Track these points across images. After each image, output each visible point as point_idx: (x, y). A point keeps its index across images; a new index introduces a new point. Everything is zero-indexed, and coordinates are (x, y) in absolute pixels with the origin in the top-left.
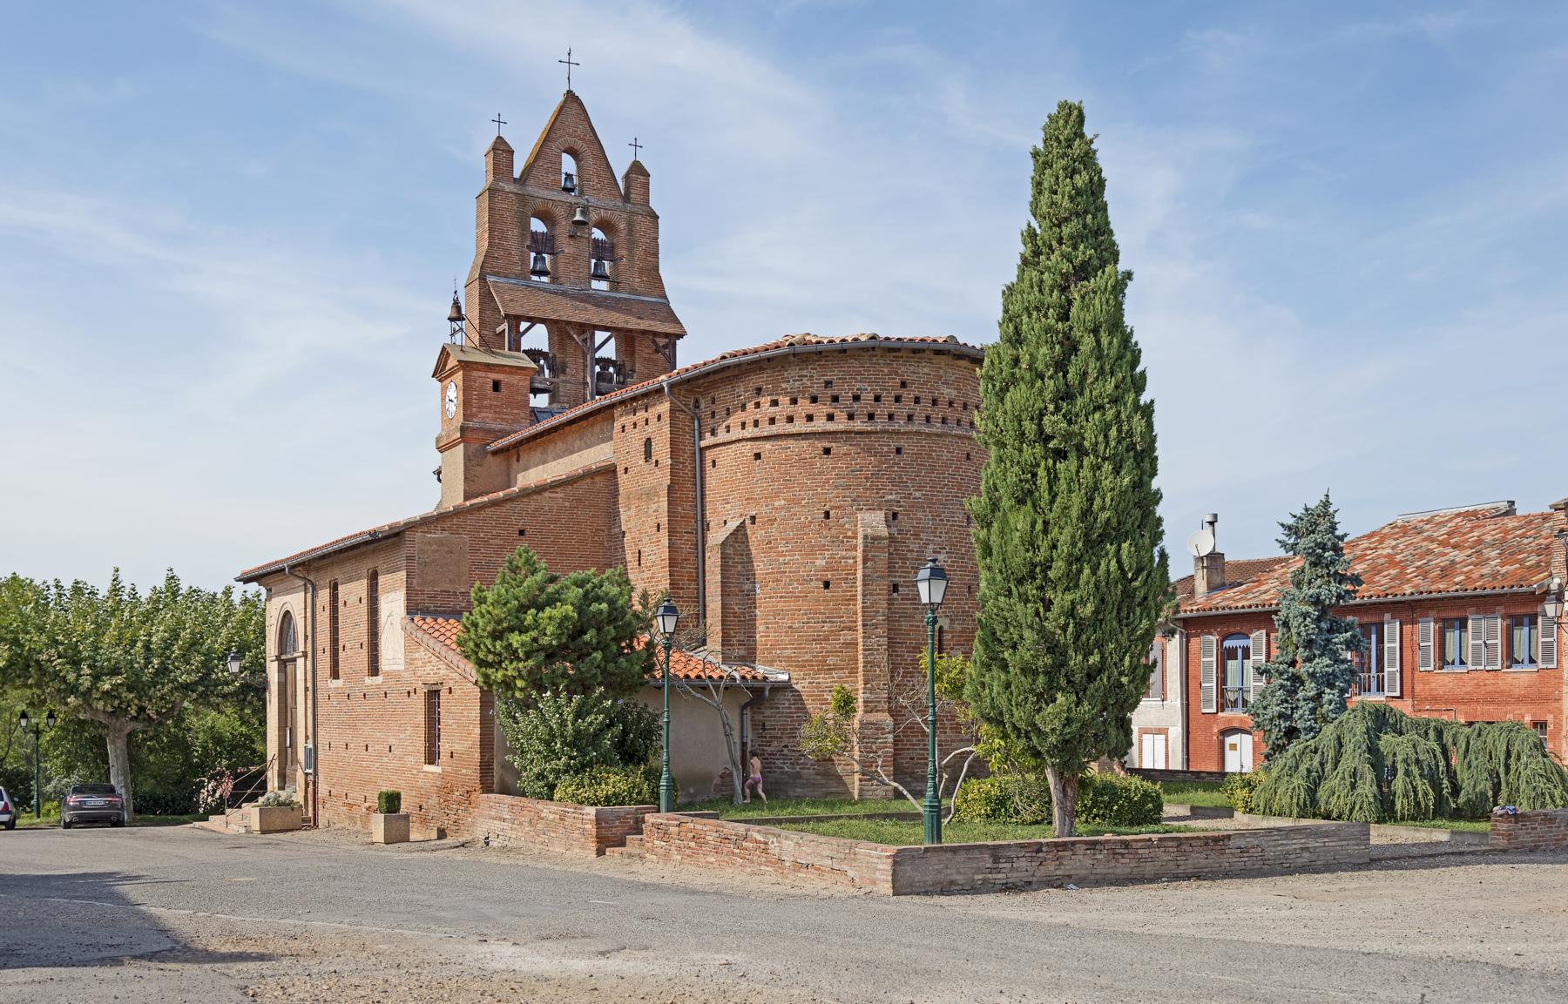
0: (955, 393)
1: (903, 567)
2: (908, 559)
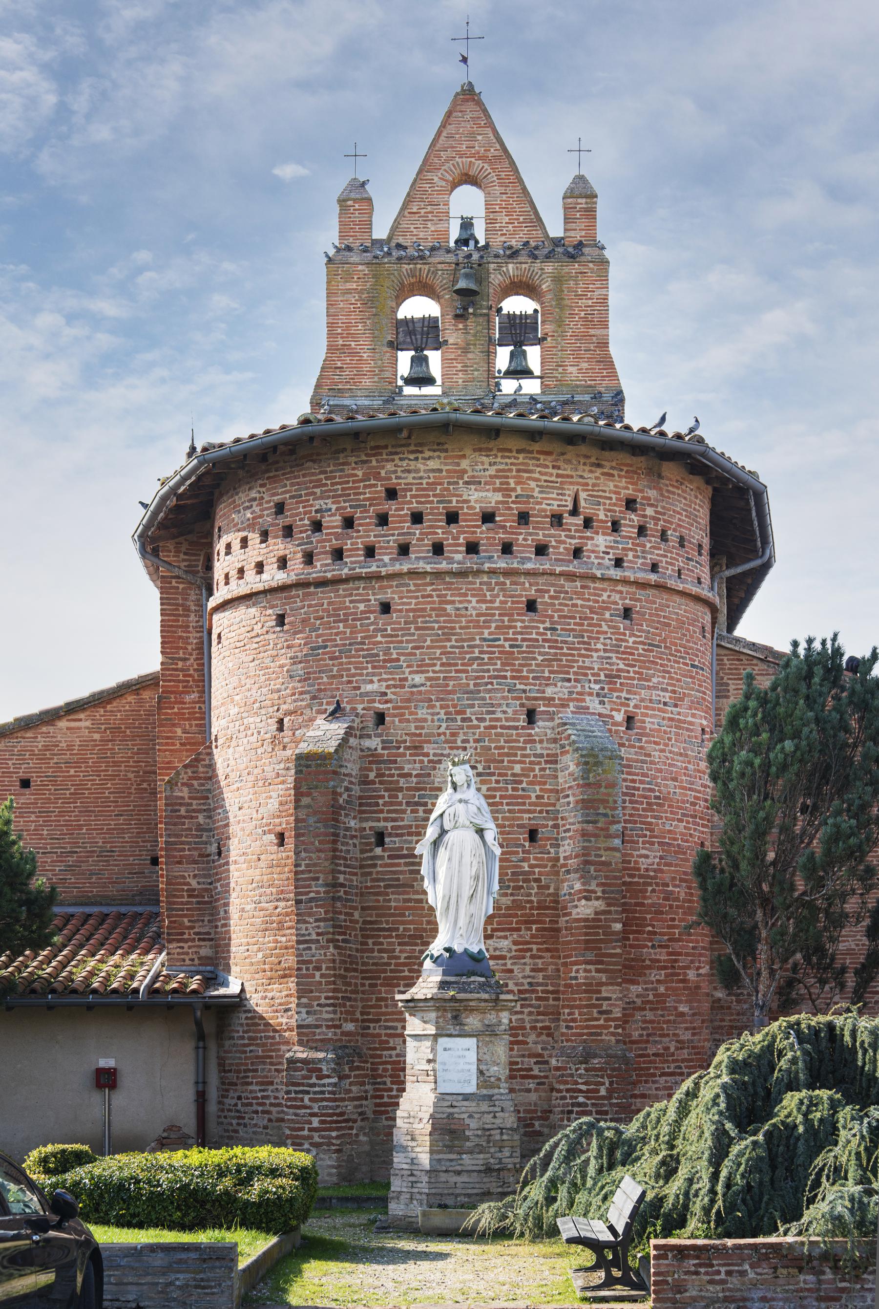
0: (499, 497)
1: (391, 804)
2: (401, 789)
